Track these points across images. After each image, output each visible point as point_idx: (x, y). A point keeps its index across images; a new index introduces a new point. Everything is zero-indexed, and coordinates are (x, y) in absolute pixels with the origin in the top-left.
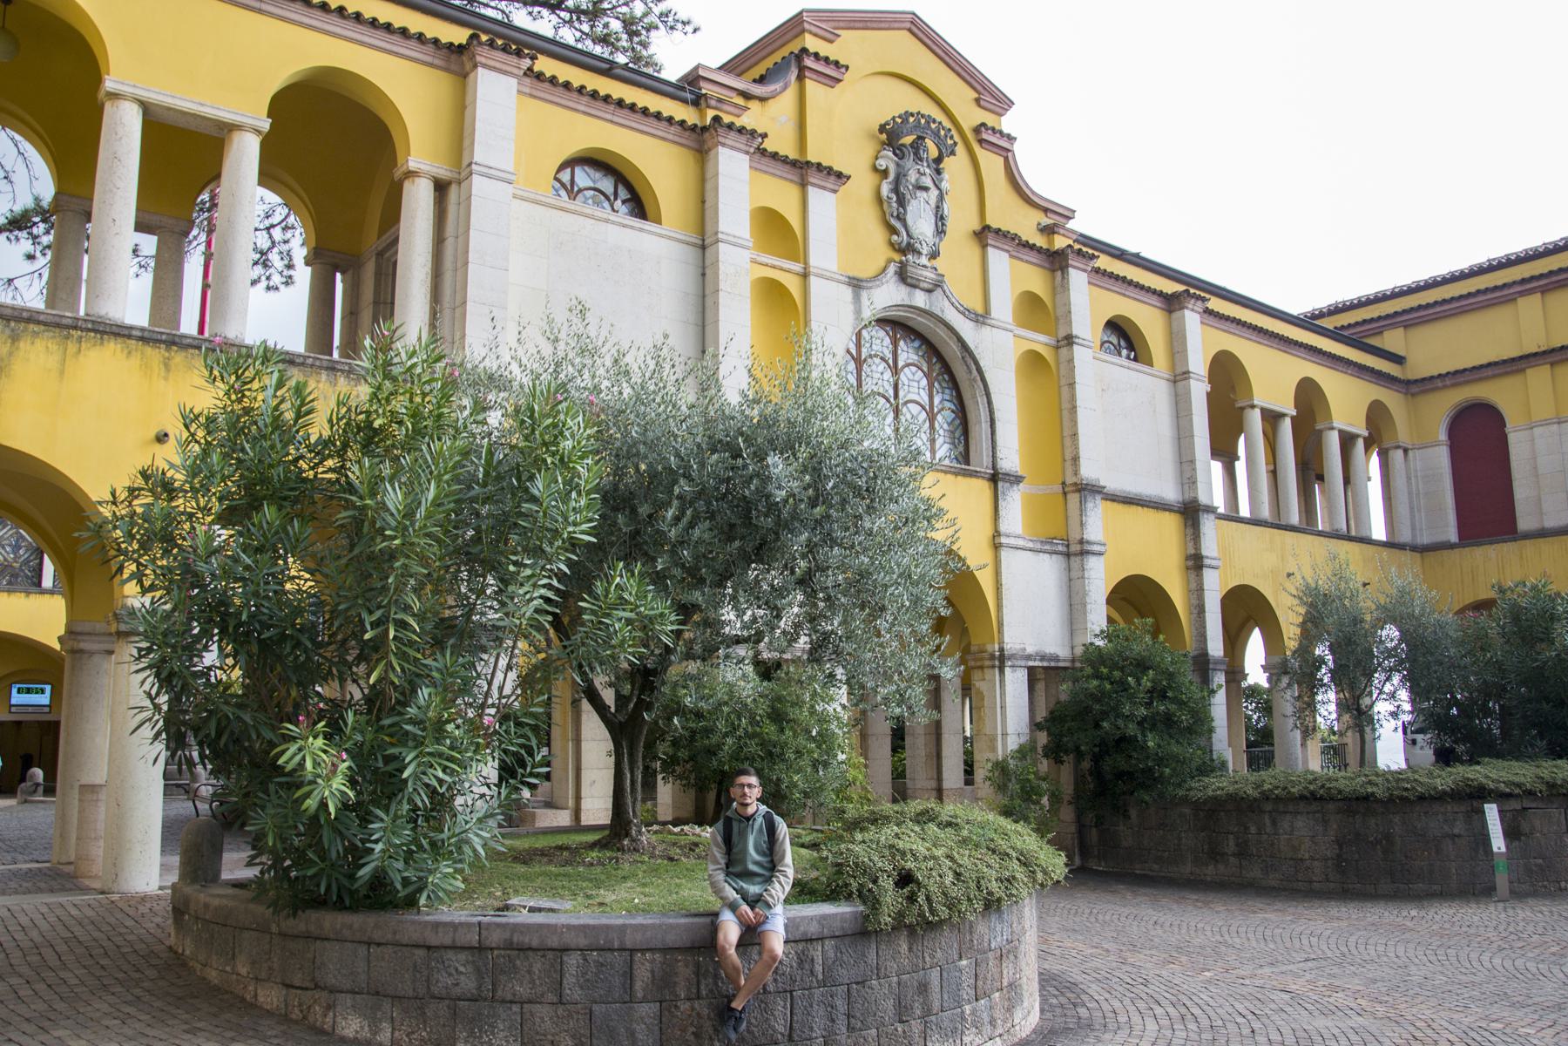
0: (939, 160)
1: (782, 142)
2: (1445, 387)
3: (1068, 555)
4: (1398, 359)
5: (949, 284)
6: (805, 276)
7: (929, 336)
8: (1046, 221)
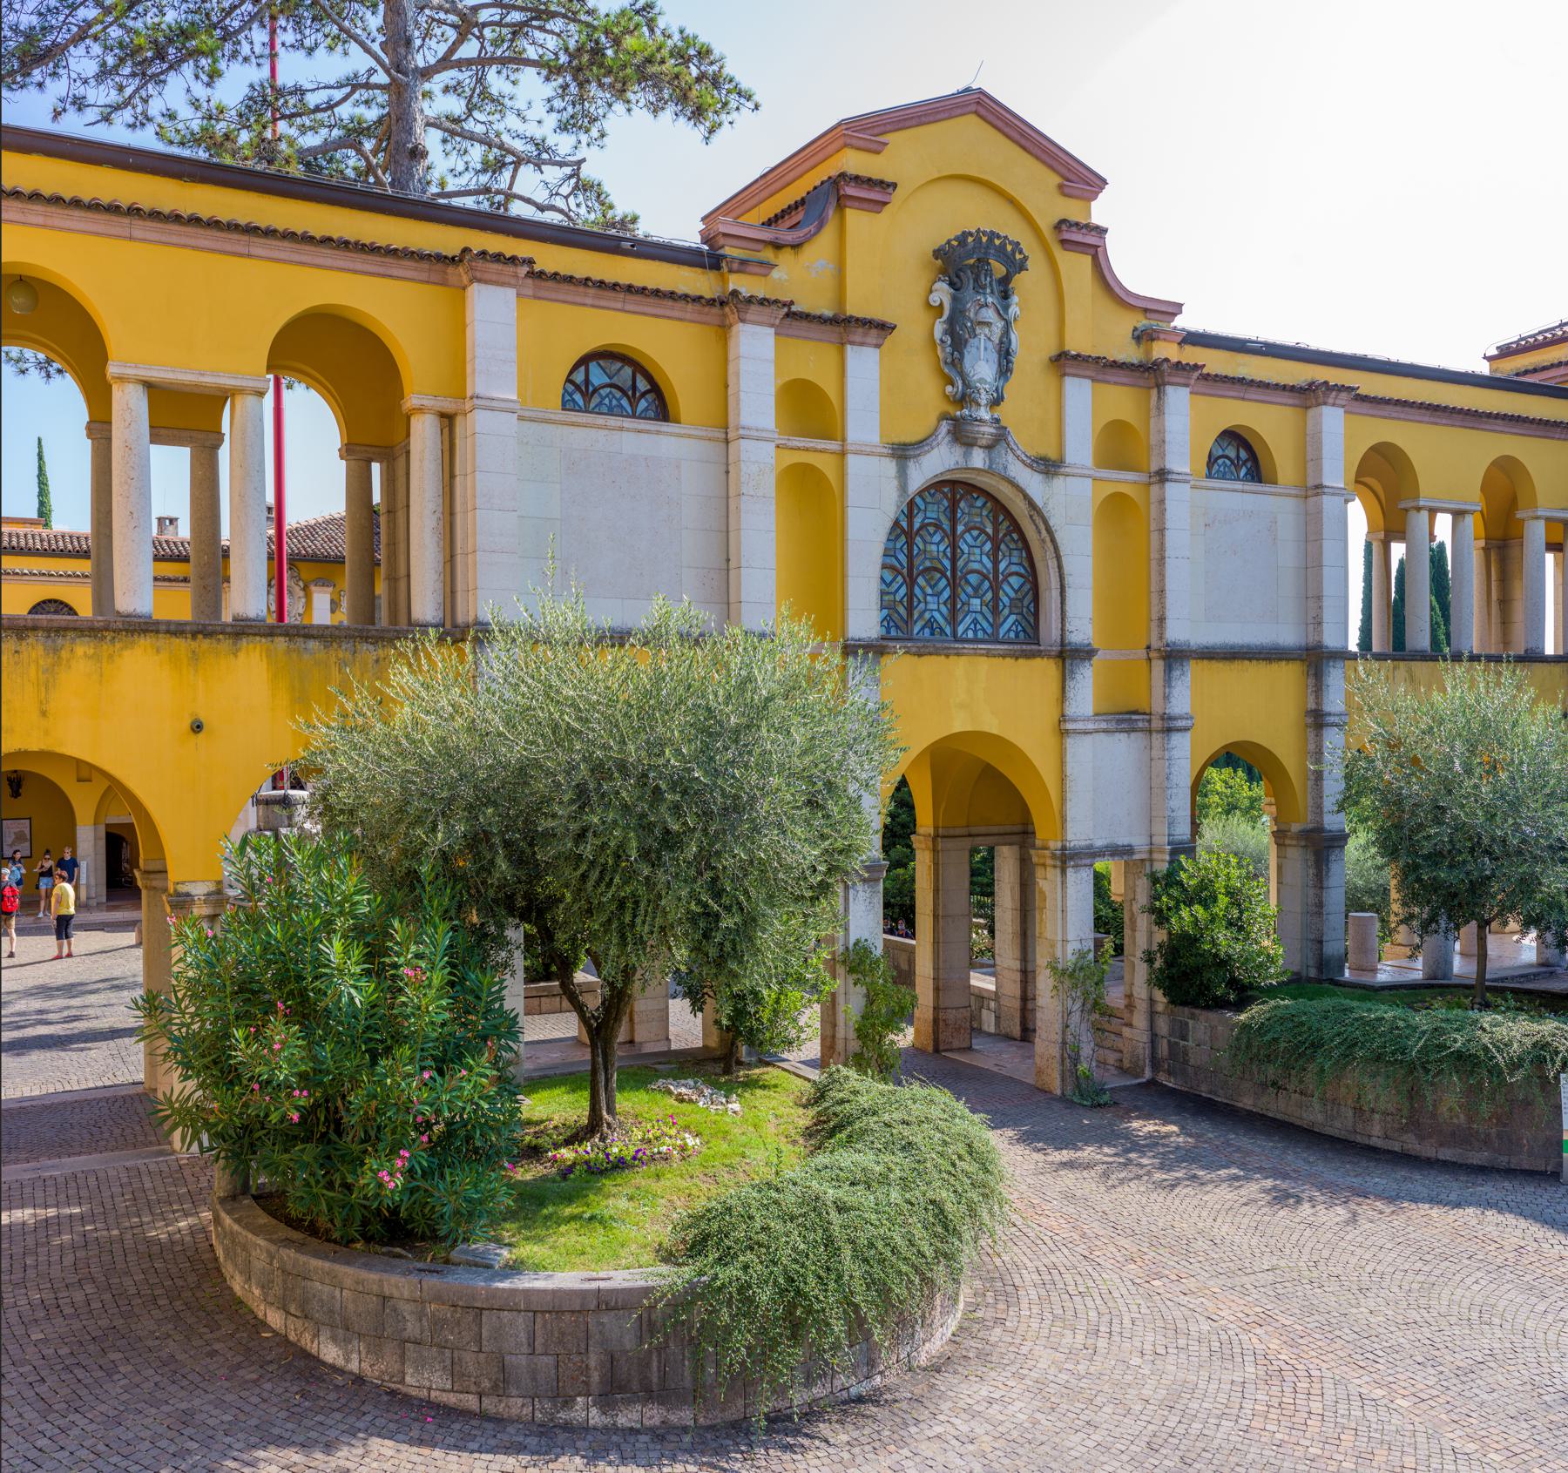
0: (1005, 281)
1: (816, 301)
5: (1015, 436)
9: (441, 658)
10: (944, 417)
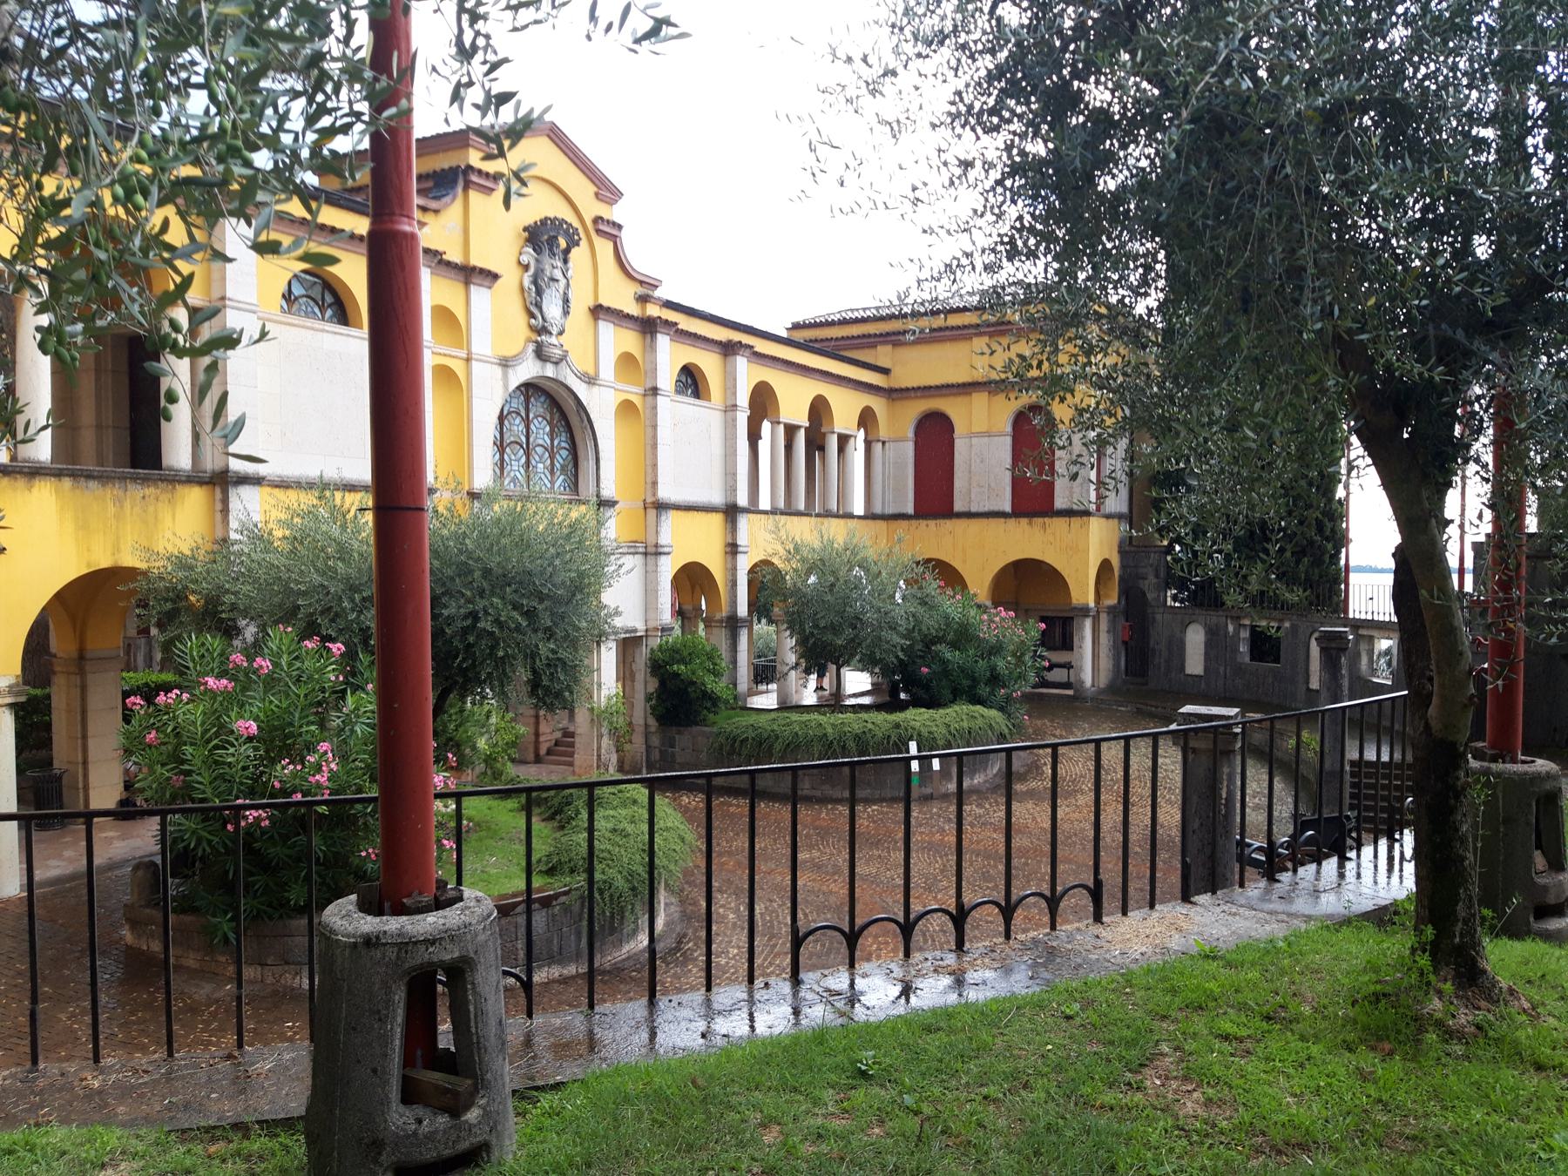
0: (567, 251)
2: (917, 397)
3: (646, 554)
4: (885, 371)
5: (572, 357)
6: (468, 360)
7: (552, 393)
8: (641, 290)
9: (194, 499)
10: (529, 340)
